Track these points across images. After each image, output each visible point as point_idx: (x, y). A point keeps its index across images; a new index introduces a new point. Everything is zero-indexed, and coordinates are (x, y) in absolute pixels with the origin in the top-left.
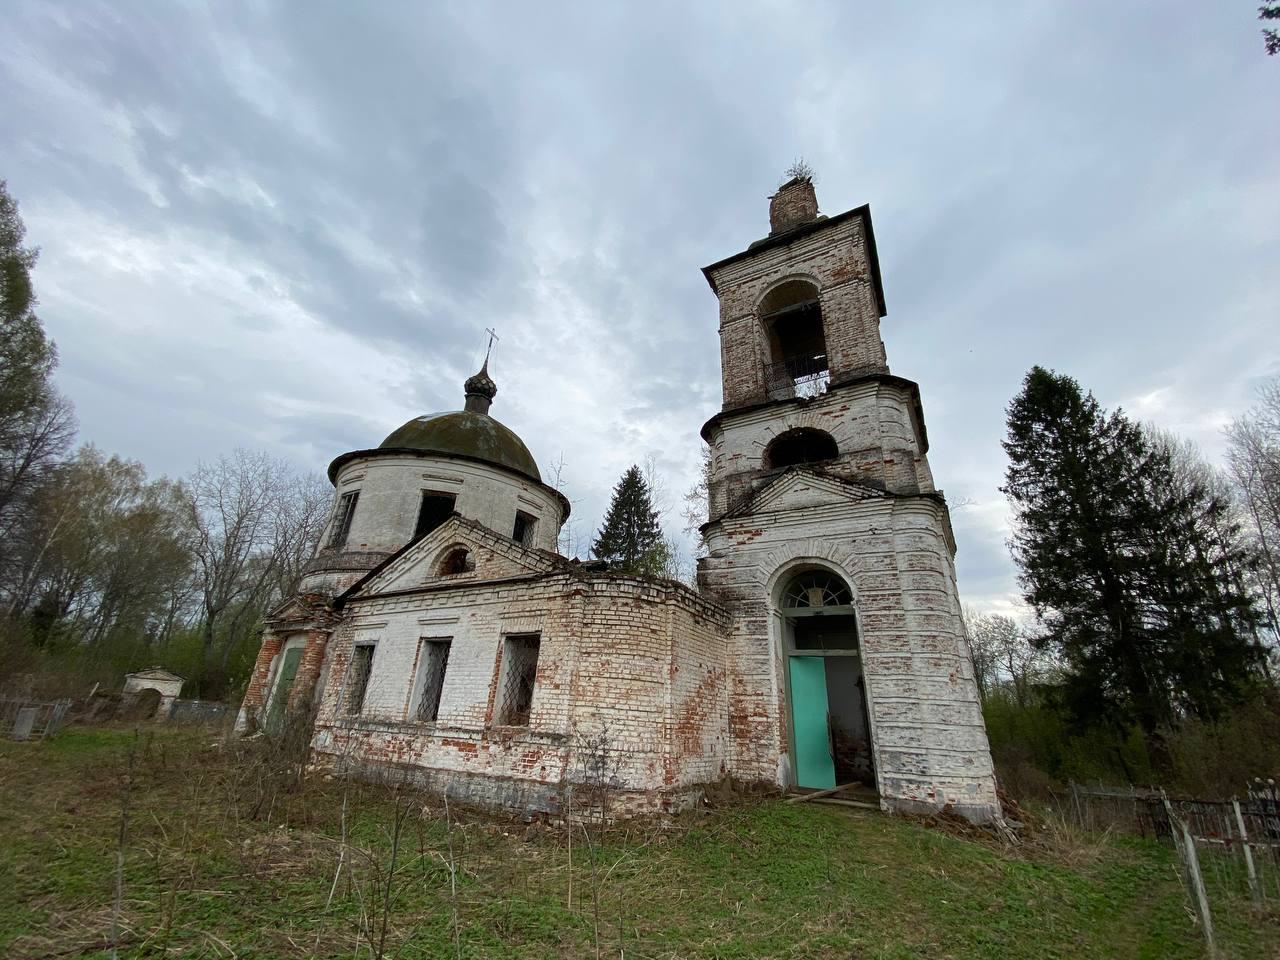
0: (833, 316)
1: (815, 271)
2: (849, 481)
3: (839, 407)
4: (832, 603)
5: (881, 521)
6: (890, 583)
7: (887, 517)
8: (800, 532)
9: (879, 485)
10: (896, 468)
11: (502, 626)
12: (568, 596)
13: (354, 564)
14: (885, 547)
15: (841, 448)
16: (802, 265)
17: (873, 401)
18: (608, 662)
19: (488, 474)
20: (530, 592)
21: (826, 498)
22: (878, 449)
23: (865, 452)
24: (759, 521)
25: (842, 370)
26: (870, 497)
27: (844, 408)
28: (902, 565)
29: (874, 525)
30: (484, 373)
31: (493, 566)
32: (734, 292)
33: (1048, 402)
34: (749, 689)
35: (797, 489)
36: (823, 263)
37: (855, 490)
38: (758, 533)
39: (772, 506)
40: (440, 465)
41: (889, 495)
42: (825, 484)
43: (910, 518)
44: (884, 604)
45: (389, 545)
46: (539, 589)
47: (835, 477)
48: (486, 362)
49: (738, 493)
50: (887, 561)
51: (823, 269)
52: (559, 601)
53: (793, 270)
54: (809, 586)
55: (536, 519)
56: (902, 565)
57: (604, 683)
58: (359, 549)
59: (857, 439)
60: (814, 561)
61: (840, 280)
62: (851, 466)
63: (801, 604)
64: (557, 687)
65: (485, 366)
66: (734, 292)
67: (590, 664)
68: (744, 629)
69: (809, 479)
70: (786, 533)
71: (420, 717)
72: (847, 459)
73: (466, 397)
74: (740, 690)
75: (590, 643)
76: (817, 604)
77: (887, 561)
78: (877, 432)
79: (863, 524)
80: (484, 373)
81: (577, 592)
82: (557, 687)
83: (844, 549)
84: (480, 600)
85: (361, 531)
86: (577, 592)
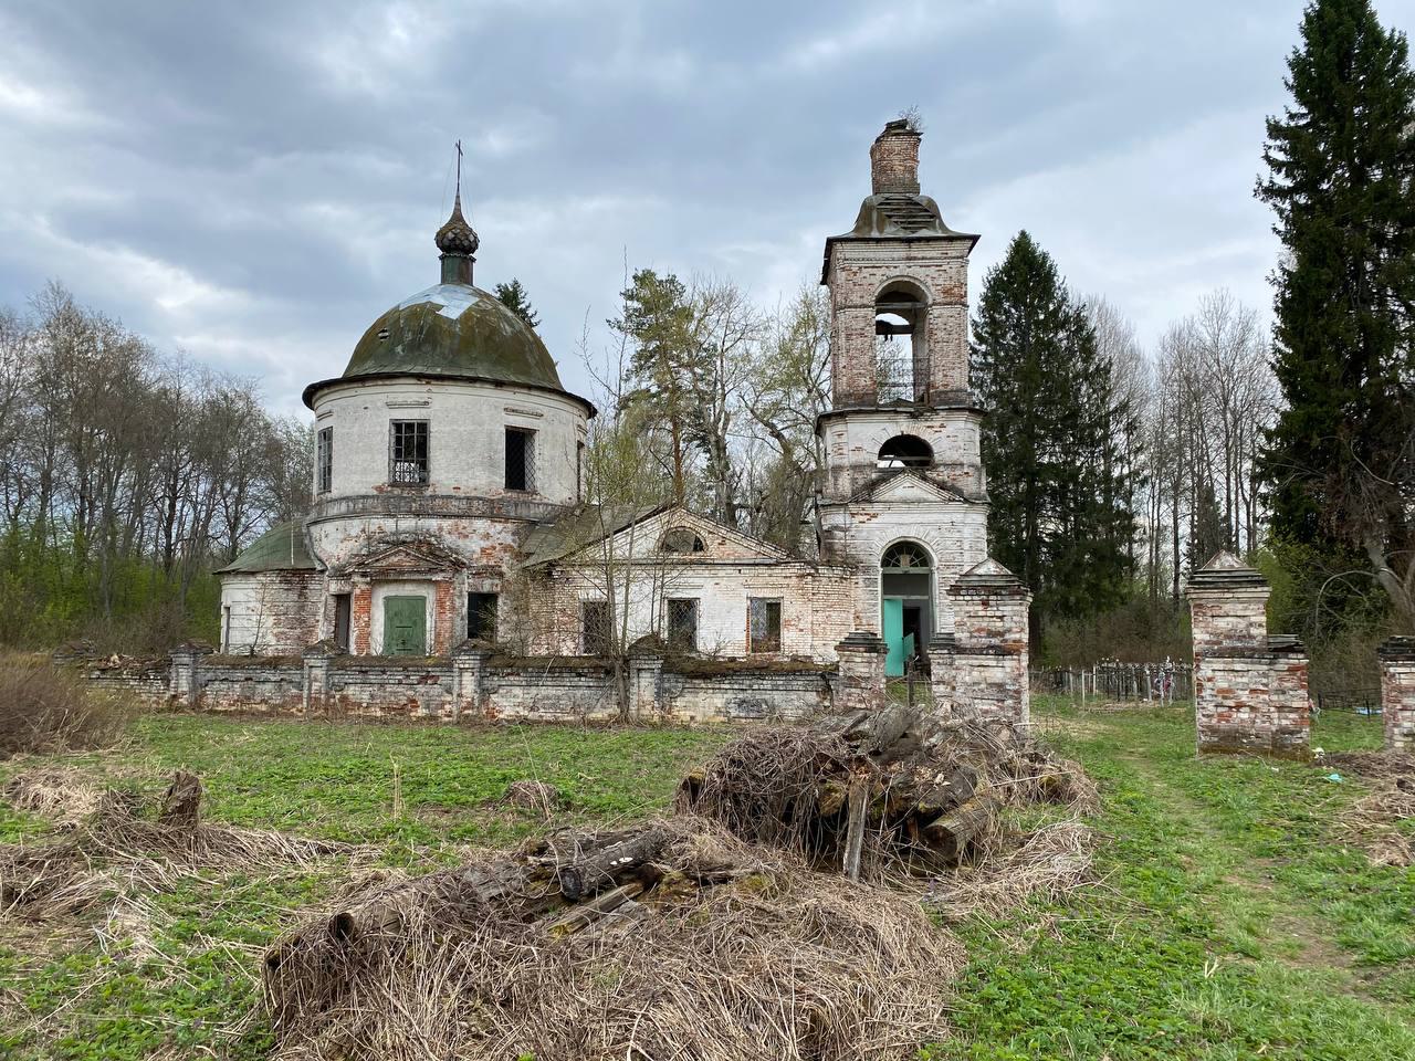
0: (940, 335)
1: (930, 282)
2: (942, 486)
3: (938, 424)
4: (916, 565)
5: (958, 517)
6: (958, 558)
7: (962, 515)
8: (907, 518)
9: (959, 492)
10: (970, 479)
12: (802, 576)
14: (958, 535)
15: (937, 458)
16: (918, 269)
18: (830, 616)
20: (770, 571)
22: (962, 465)
23: (954, 465)
24: (877, 508)
25: (941, 388)
26: (954, 500)
27: (942, 426)
28: (966, 547)
29: (954, 520)
30: (457, 217)
31: (729, 547)
32: (855, 273)
33: (1026, 274)
34: (864, 622)
35: (907, 487)
36: (936, 275)
37: (946, 494)
38: (875, 516)
39: (887, 497)
40: (518, 396)
41: (966, 501)
42: (925, 486)
43: (975, 516)
44: (953, 571)
45: (486, 489)
47: (934, 482)
48: (458, 197)
49: (861, 482)
50: (959, 544)
51: (936, 282)
52: (794, 579)
53: (907, 271)
54: (901, 553)
56: (966, 547)
57: (828, 627)
58: (452, 493)
59: (948, 453)
60: (912, 540)
61: (948, 300)
62: (943, 475)
63: (894, 565)
64: (802, 630)
66: (855, 273)
67: (820, 616)
68: (861, 583)
69: (916, 480)
70: (895, 518)
72: (941, 469)
73: (442, 258)
74: (858, 622)
75: (819, 605)
76: (905, 565)
77: (959, 544)
78: (962, 451)
79: (947, 518)
80: (457, 217)
81: (809, 574)
82: (802, 630)
83: (933, 533)
84: (721, 573)
85: (448, 472)
86: (809, 574)
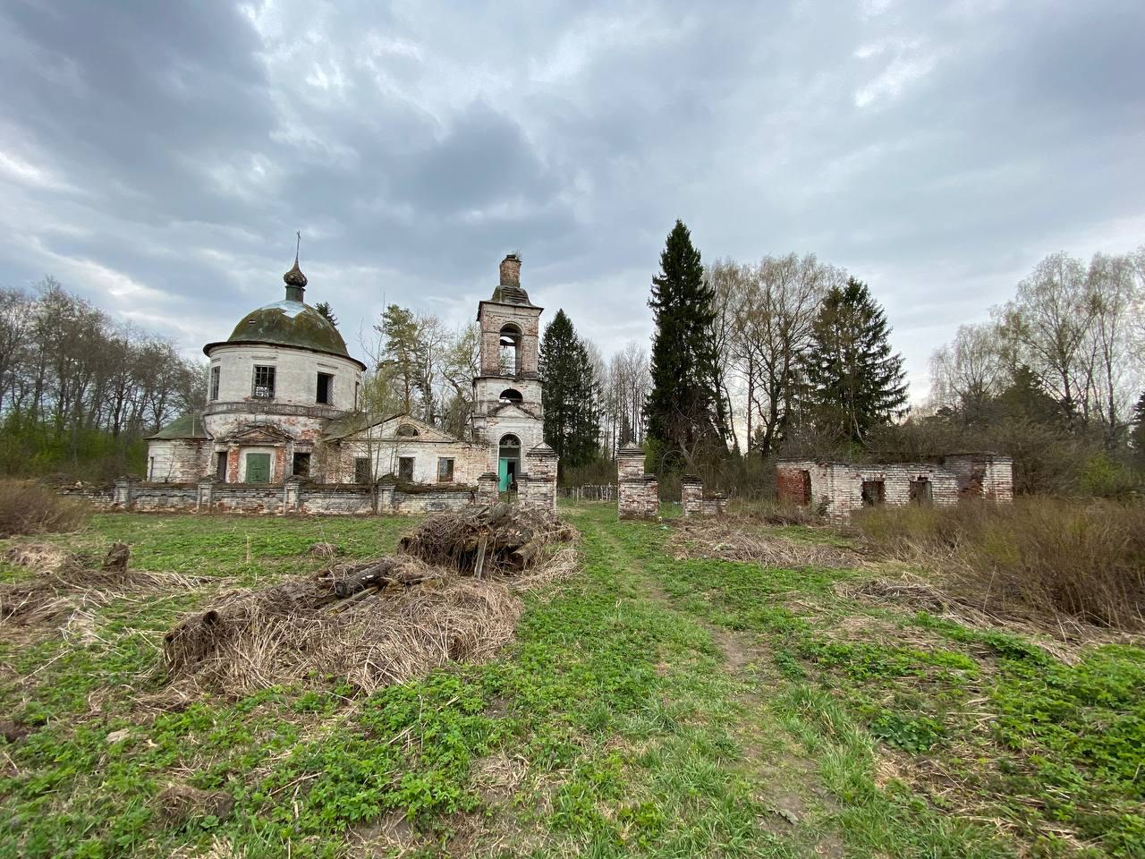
2: (526, 411)
5: (532, 425)
11: (437, 455)
12: (464, 448)
13: (288, 412)
17: (534, 386)
19: (348, 364)
21: (518, 415)
30: (296, 268)
31: (430, 434)
37: (527, 415)
40: (325, 358)
42: (519, 411)
46: (453, 445)
55: (333, 375)
58: (287, 403)
62: (526, 407)
65: (297, 262)
69: (515, 409)
71: (294, 473)
76: (509, 444)
79: (527, 425)
80: (296, 268)
84: (426, 446)
